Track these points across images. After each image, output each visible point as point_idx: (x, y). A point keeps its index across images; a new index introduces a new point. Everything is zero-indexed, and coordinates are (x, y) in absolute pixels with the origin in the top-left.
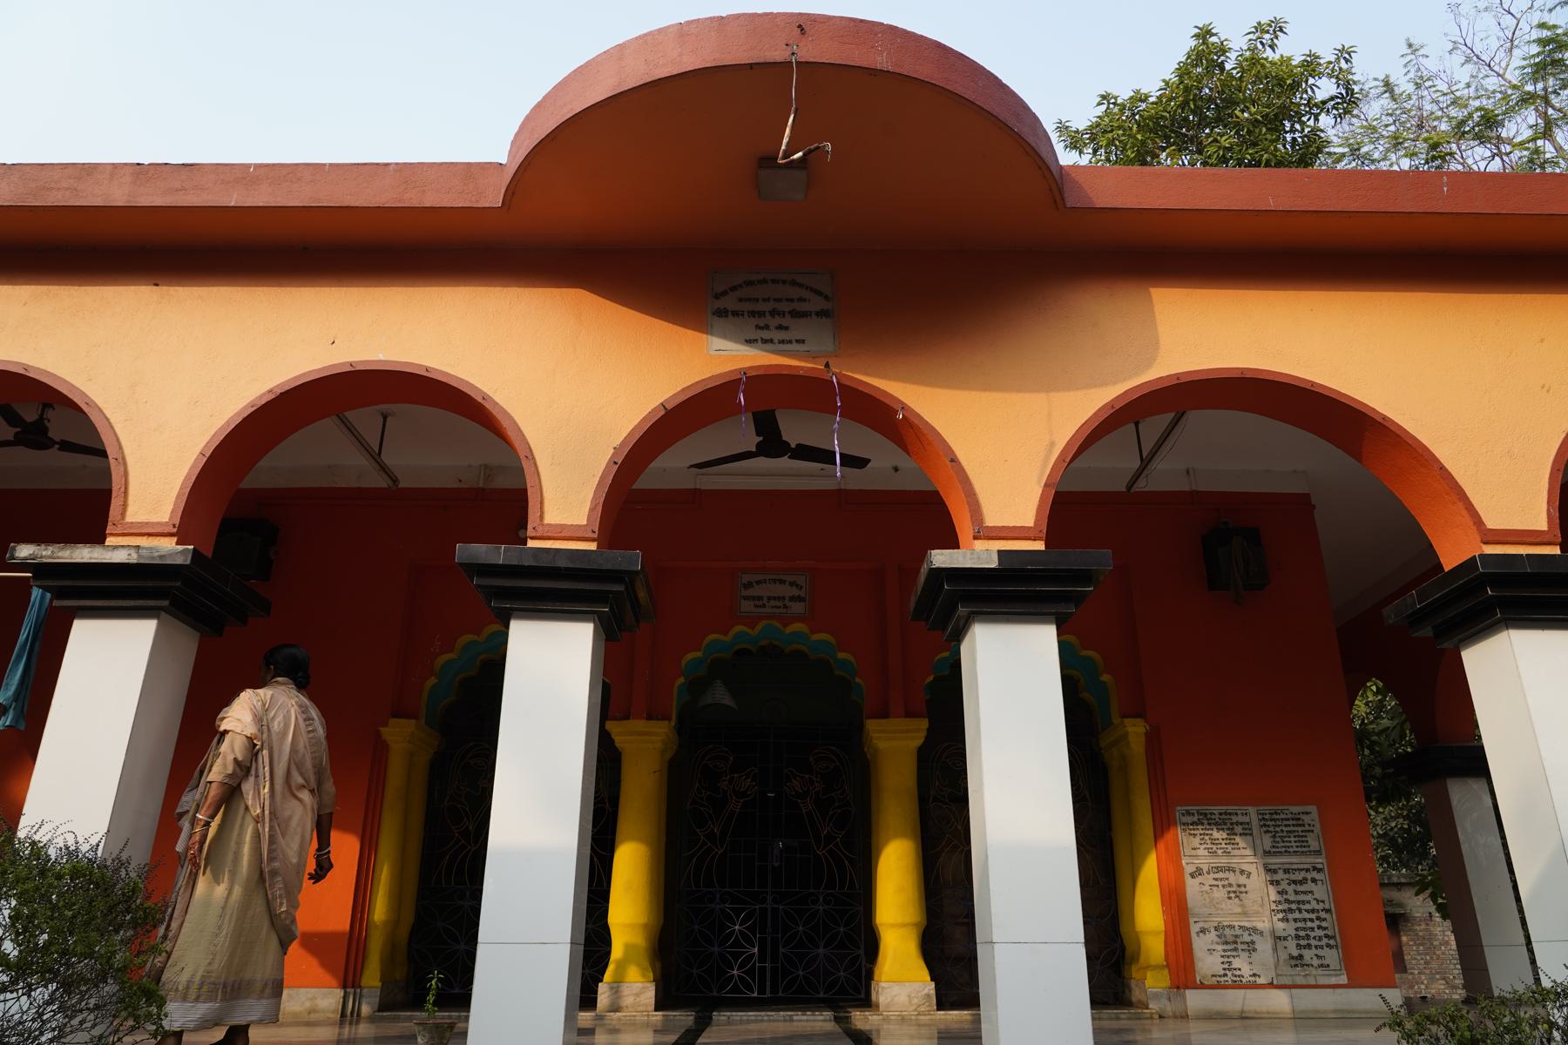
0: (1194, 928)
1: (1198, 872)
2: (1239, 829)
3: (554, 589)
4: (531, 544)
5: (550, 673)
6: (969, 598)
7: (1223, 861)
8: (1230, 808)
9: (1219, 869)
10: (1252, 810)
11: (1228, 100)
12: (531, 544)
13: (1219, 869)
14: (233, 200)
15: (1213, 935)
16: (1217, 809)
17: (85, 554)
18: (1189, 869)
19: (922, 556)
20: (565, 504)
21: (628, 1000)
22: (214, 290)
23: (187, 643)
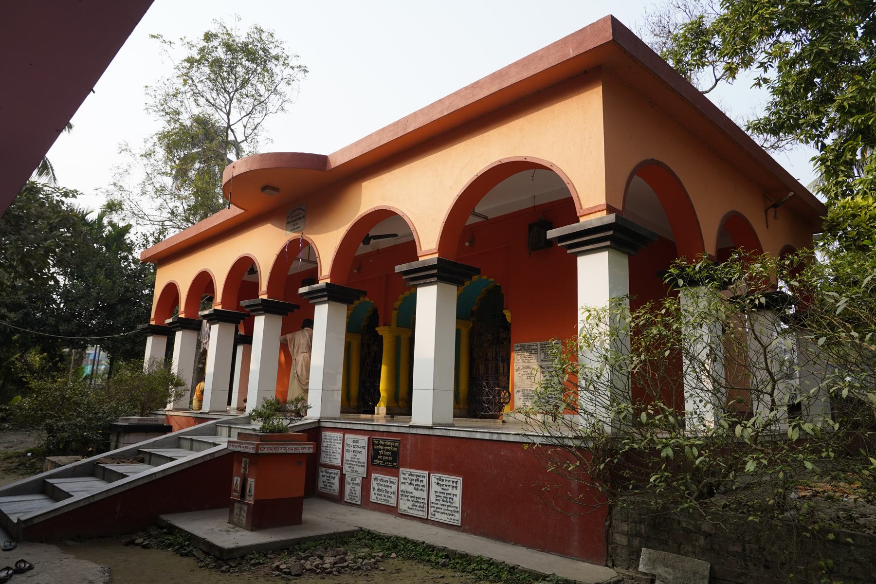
0: (516, 390)
1: (519, 369)
2: (533, 352)
3: (591, 240)
4: (421, 259)
5: (428, 301)
6: (252, 311)
7: (526, 364)
8: (531, 343)
9: (526, 368)
10: (539, 343)
11: (135, 273)
12: (260, 297)
13: (526, 368)
14: (531, 73)
15: (520, 393)
16: (527, 344)
17: (315, 286)
18: (516, 368)
19: (297, 291)
20: (428, 243)
21: (380, 412)
22: (540, 112)
23: (625, 261)
